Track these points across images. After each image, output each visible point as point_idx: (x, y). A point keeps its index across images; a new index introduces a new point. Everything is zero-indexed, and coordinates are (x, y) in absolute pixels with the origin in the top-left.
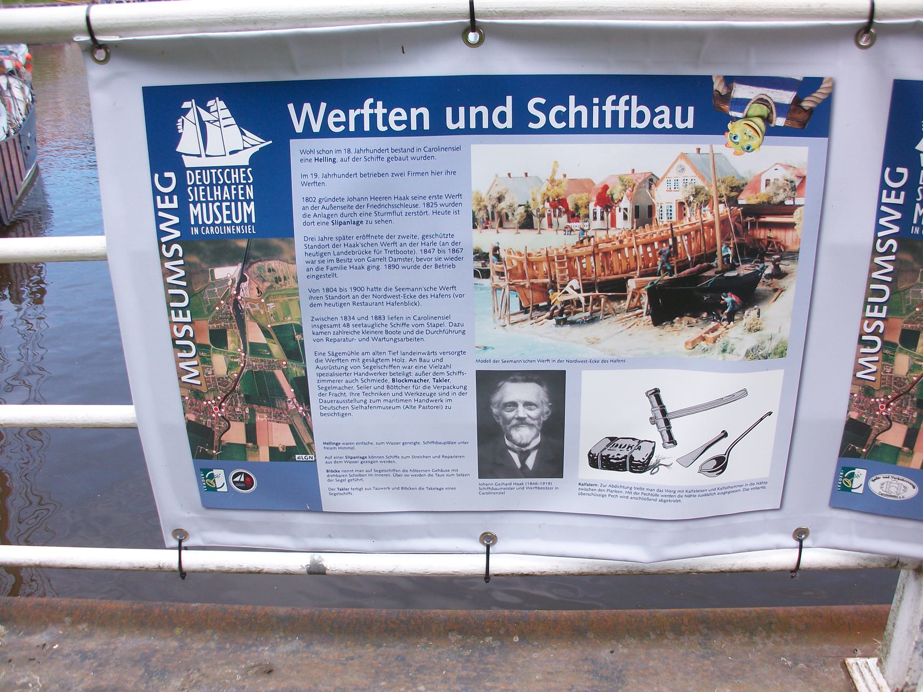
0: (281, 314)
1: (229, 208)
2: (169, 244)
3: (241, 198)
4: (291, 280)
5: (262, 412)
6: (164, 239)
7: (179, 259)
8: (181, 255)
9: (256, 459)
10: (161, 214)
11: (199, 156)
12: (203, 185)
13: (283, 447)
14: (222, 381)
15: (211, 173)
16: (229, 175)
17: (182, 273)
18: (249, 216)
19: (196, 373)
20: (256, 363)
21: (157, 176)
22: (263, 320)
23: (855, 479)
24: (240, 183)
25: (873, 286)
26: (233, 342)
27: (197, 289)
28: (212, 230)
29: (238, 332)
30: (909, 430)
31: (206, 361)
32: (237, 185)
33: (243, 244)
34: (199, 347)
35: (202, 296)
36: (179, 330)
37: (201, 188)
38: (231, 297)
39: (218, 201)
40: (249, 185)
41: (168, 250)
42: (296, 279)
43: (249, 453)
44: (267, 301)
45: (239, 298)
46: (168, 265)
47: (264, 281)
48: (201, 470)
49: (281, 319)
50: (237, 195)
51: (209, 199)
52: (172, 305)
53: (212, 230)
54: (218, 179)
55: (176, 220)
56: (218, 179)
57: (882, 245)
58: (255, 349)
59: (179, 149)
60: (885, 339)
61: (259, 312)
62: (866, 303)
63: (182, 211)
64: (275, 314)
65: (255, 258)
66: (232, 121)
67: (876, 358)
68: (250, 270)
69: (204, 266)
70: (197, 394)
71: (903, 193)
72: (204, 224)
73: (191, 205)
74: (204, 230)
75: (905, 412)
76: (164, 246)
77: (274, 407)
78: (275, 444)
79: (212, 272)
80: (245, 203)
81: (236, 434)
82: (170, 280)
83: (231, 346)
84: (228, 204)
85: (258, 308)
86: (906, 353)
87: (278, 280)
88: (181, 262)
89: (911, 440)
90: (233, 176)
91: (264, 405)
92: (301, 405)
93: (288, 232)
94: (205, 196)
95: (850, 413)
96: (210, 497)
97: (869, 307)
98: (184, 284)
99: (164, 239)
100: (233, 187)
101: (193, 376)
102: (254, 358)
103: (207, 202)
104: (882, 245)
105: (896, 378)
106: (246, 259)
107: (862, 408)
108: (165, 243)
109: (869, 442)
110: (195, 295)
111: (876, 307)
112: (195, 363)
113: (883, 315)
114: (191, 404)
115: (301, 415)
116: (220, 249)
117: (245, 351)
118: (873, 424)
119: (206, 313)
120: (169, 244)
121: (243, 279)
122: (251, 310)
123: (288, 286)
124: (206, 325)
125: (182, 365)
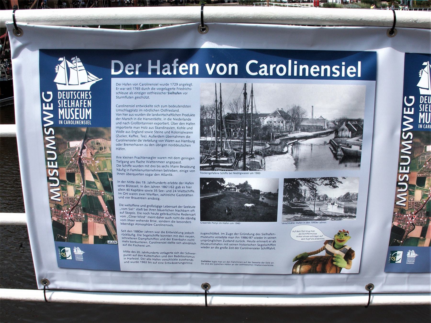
0: (102, 167)
1: (78, 111)
2: (48, 128)
3: (84, 106)
4: (108, 149)
5: (91, 217)
6: (45, 125)
7: (52, 135)
8: (53, 133)
9: (87, 243)
10: (44, 112)
11: (65, 84)
12: (66, 99)
13: (101, 236)
14: (72, 200)
15: (70, 94)
16: (80, 94)
17: (54, 143)
18: (88, 116)
19: (59, 195)
20: (89, 192)
21: (43, 93)
22: (93, 170)
23: (397, 257)
24: (85, 99)
25: (402, 157)
26: (78, 179)
27: (61, 151)
28: (69, 122)
29: (80, 174)
30: (423, 228)
31: (64, 189)
32: (83, 100)
33: (84, 130)
34: (61, 181)
35: (64, 155)
36: (51, 172)
37: (65, 101)
38: (78, 156)
39: (73, 107)
40: (89, 100)
41: (47, 131)
42: (110, 149)
43: (83, 239)
44: (96, 159)
45: (82, 157)
46: (47, 138)
47: (94, 149)
48: (59, 247)
49: (102, 169)
50: (83, 105)
51: (69, 106)
52: (48, 159)
53: (69, 122)
54: (74, 96)
55: (52, 116)
56: (74, 96)
57: (405, 135)
58: (89, 184)
59: (55, 81)
60: (410, 183)
61: (91, 165)
62: (399, 165)
63: (55, 112)
64: (99, 167)
65: (90, 137)
66: (83, 68)
67: (405, 194)
68: (87, 143)
69: (65, 140)
70: (58, 207)
71: (413, 109)
72: (65, 119)
73: (59, 109)
74: (65, 122)
75: (421, 219)
76: (45, 129)
77: (97, 215)
78: (97, 235)
79: (69, 143)
80: (86, 109)
81: (77, 229)
82: (48, 146)
83: (77, 182)
84: (78, 109)
85: (90, 163)
86: (420, 189)
87: (101, 149)
88: (53, 137)
89: (424, 233)
90: (81, 95)
91: (92, 213)
92: (111, 214)
93: (107, 124)
94: (67, 105)
95: (394, 223)
96: (63, 263)
97: (401, 168)
98: (55, 148)
99: (45, 125)
100: (81, 101)
101: (57, 196)
102: (88, 189)
103: (67, 108)
104: (405, 135)
105: (416, 203)
106: (85, 137)
107: (400, 220)
108: (46, 127)
109: (404, 238)
110: (60, 155)
111: (404, 167)
112: (58, 189)
113: (408, 171)
114: (55, 212)
115: (111, 220)
116: (73, 132)
117: (84, 184)
118: (406, 228)
119: (65, 164)
120: (48, 128)
121: (84, 148)
122: (88, 164)
123: (106, 153)
124: (65, 170)
125: (52, 191)
